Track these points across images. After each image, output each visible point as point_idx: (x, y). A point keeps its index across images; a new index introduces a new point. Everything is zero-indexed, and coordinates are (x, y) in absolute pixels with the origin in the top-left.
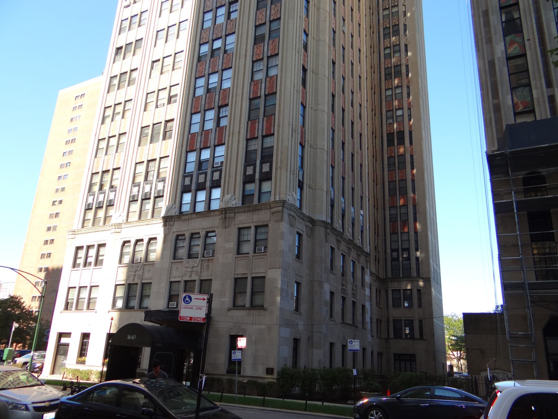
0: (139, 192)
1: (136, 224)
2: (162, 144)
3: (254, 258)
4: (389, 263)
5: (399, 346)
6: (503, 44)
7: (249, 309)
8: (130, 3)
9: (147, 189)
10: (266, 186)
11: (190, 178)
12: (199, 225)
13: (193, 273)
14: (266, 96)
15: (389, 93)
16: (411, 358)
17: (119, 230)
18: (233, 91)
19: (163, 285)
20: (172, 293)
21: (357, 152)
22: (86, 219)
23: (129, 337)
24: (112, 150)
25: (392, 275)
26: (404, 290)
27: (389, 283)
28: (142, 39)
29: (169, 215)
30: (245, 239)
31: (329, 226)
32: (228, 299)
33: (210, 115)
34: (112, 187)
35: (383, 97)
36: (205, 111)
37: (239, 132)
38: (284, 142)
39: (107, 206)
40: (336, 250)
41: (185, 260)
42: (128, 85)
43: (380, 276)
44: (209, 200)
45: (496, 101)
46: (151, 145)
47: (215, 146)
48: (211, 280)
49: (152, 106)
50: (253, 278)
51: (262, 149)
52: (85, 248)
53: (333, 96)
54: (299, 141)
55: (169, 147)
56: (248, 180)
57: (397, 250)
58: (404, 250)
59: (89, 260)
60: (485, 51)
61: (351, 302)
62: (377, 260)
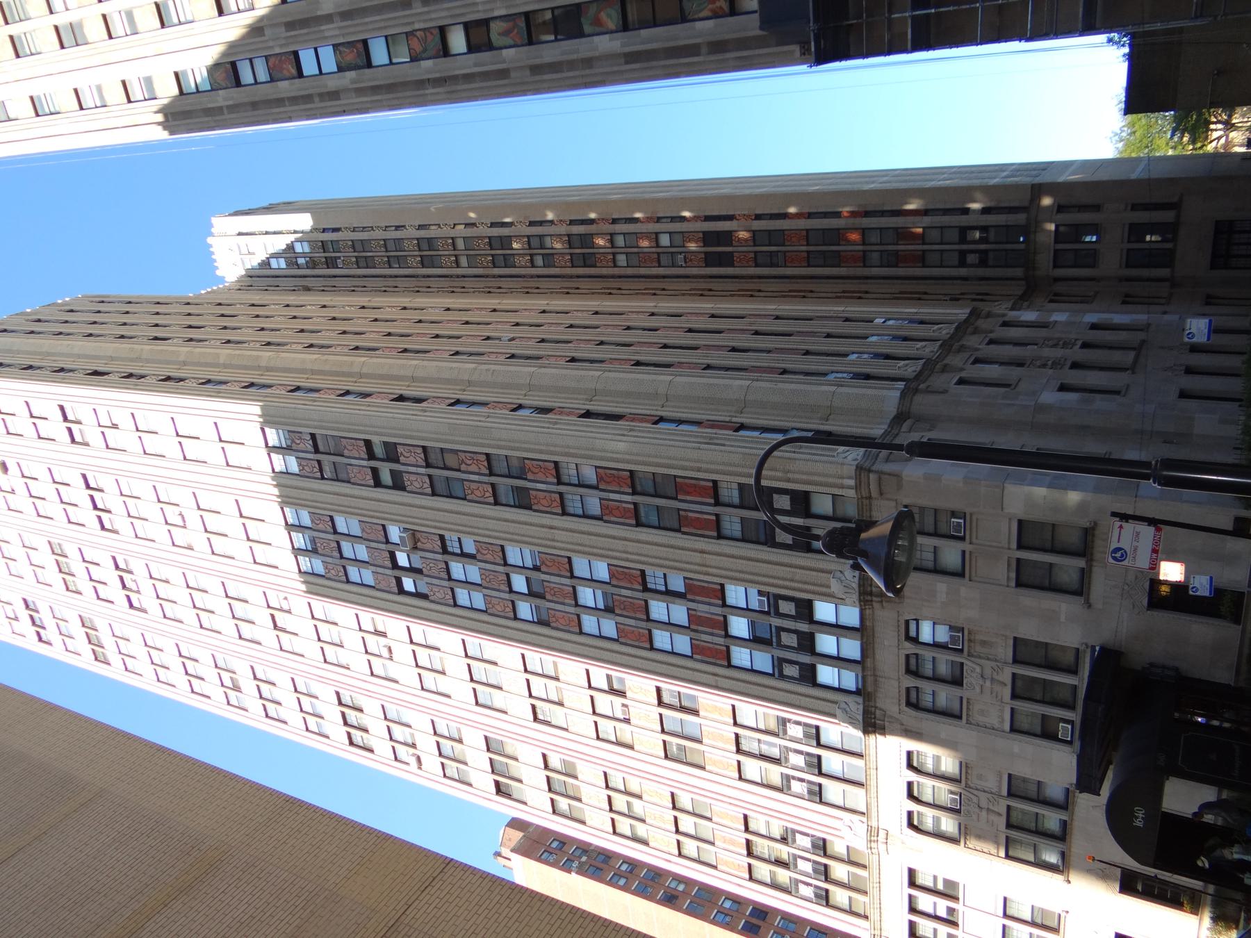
0: (802, 780)
1: (873, 795)
2: (705, 718)
3: (974, 540)
6: (596, 39)
7: (1090, 561)
8: (414, 755)
9: (799, 760)
10: (822, 505)
11: (784, 665)
12: (890, 655)
13: (995, 676)
14: (634, 493)
15: (622, 259)
17: (882, 834)
18: (616, 558)
19: (1016, 750)
20: (1038, 730)
21: (751, 324)
22: (847, 908)
23: (1139, 823)
24: (705, 828)
26: (1056, 242)
28: (486, 738)
29: (860, 718)
30: (930, 556)
31: (912, 387)
32: (1064, 606)
33: (658, 609)
34: (784, 840)
35: (630, 271)
36: (648, 619)
37: (702, 552)
38: (730, 462)
39: (825, 855)
40: (963, 374)
41: (965, 693)
42: (576, 777)
43: (1020, 293)
44: (837, 628)
45: (704, 50)
46: (704, 741)
47: (724, 605)
48: (1015, 639)
49: (625, 733)
50: (1020, 546)
51: (741, 506)
52: (914, 918)
53: (638, 363)
54: (731, 432)
55: (714, 706)
56: (803, 542)
57: (963, 254)
58: (963, 239)
59: (942, 913)
60: (608, 69)
61: (1085, 350)
62: (983, 297)
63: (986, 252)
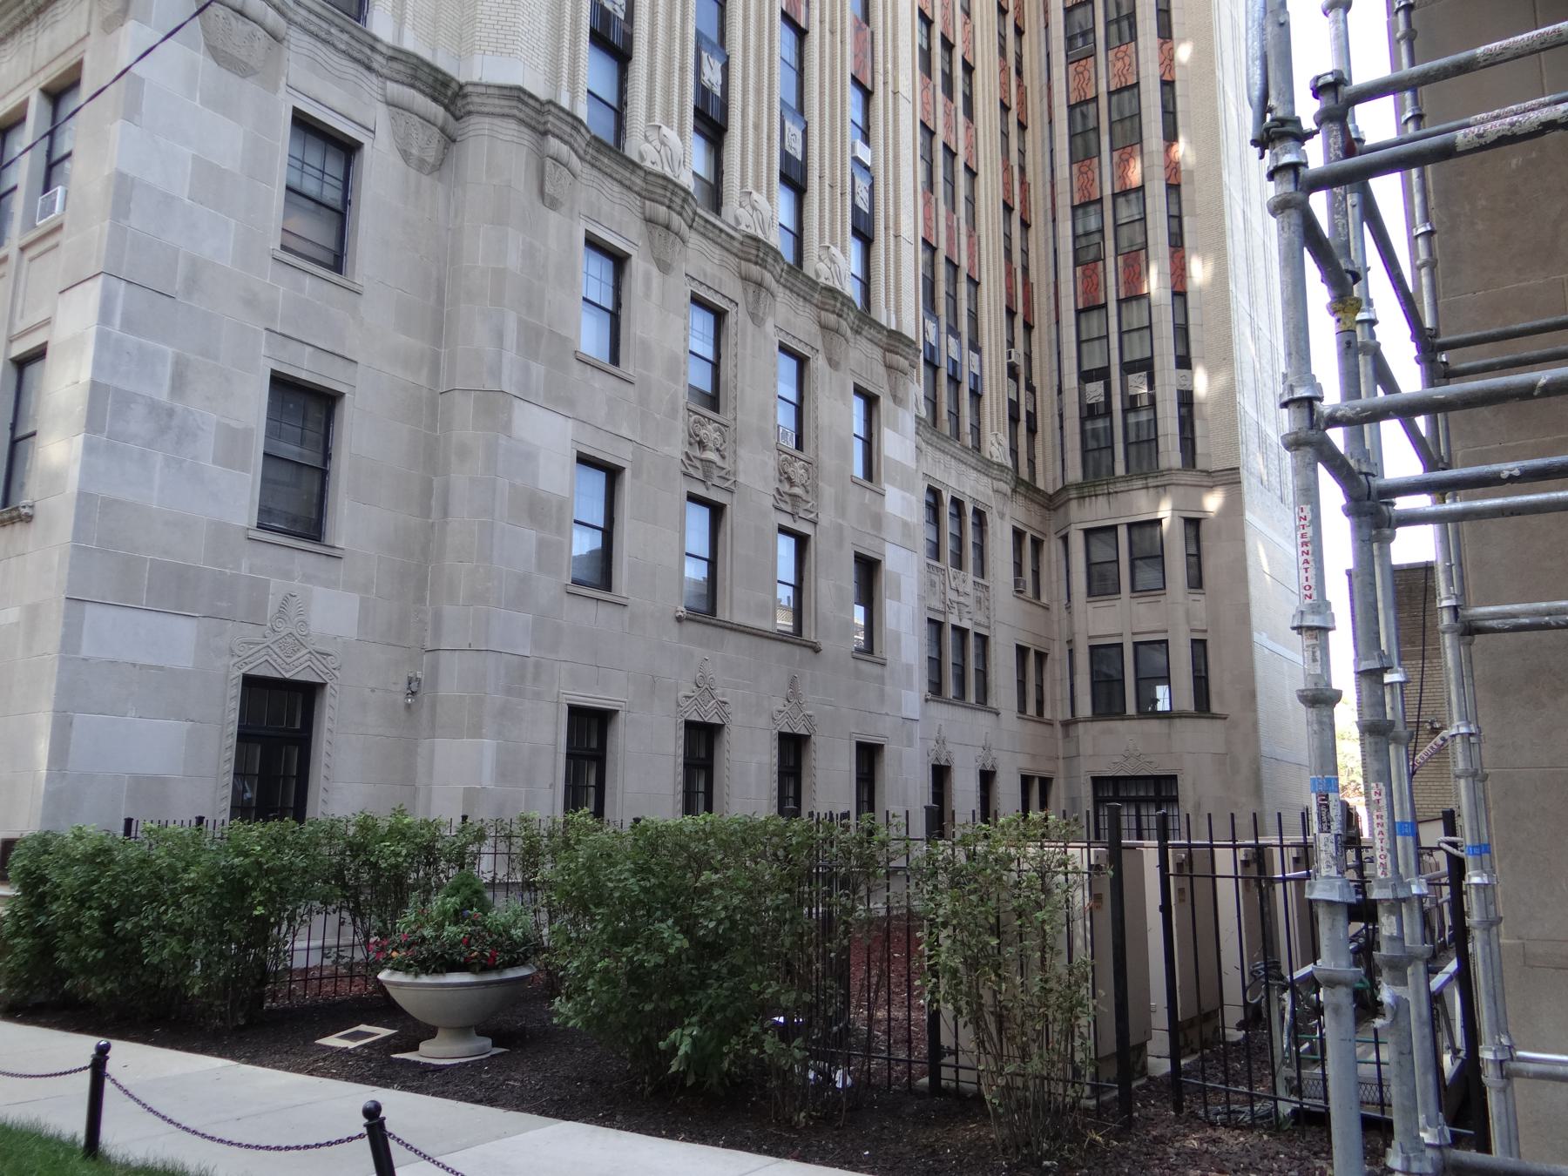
27: (1074, 504)
57: (1103, 374)
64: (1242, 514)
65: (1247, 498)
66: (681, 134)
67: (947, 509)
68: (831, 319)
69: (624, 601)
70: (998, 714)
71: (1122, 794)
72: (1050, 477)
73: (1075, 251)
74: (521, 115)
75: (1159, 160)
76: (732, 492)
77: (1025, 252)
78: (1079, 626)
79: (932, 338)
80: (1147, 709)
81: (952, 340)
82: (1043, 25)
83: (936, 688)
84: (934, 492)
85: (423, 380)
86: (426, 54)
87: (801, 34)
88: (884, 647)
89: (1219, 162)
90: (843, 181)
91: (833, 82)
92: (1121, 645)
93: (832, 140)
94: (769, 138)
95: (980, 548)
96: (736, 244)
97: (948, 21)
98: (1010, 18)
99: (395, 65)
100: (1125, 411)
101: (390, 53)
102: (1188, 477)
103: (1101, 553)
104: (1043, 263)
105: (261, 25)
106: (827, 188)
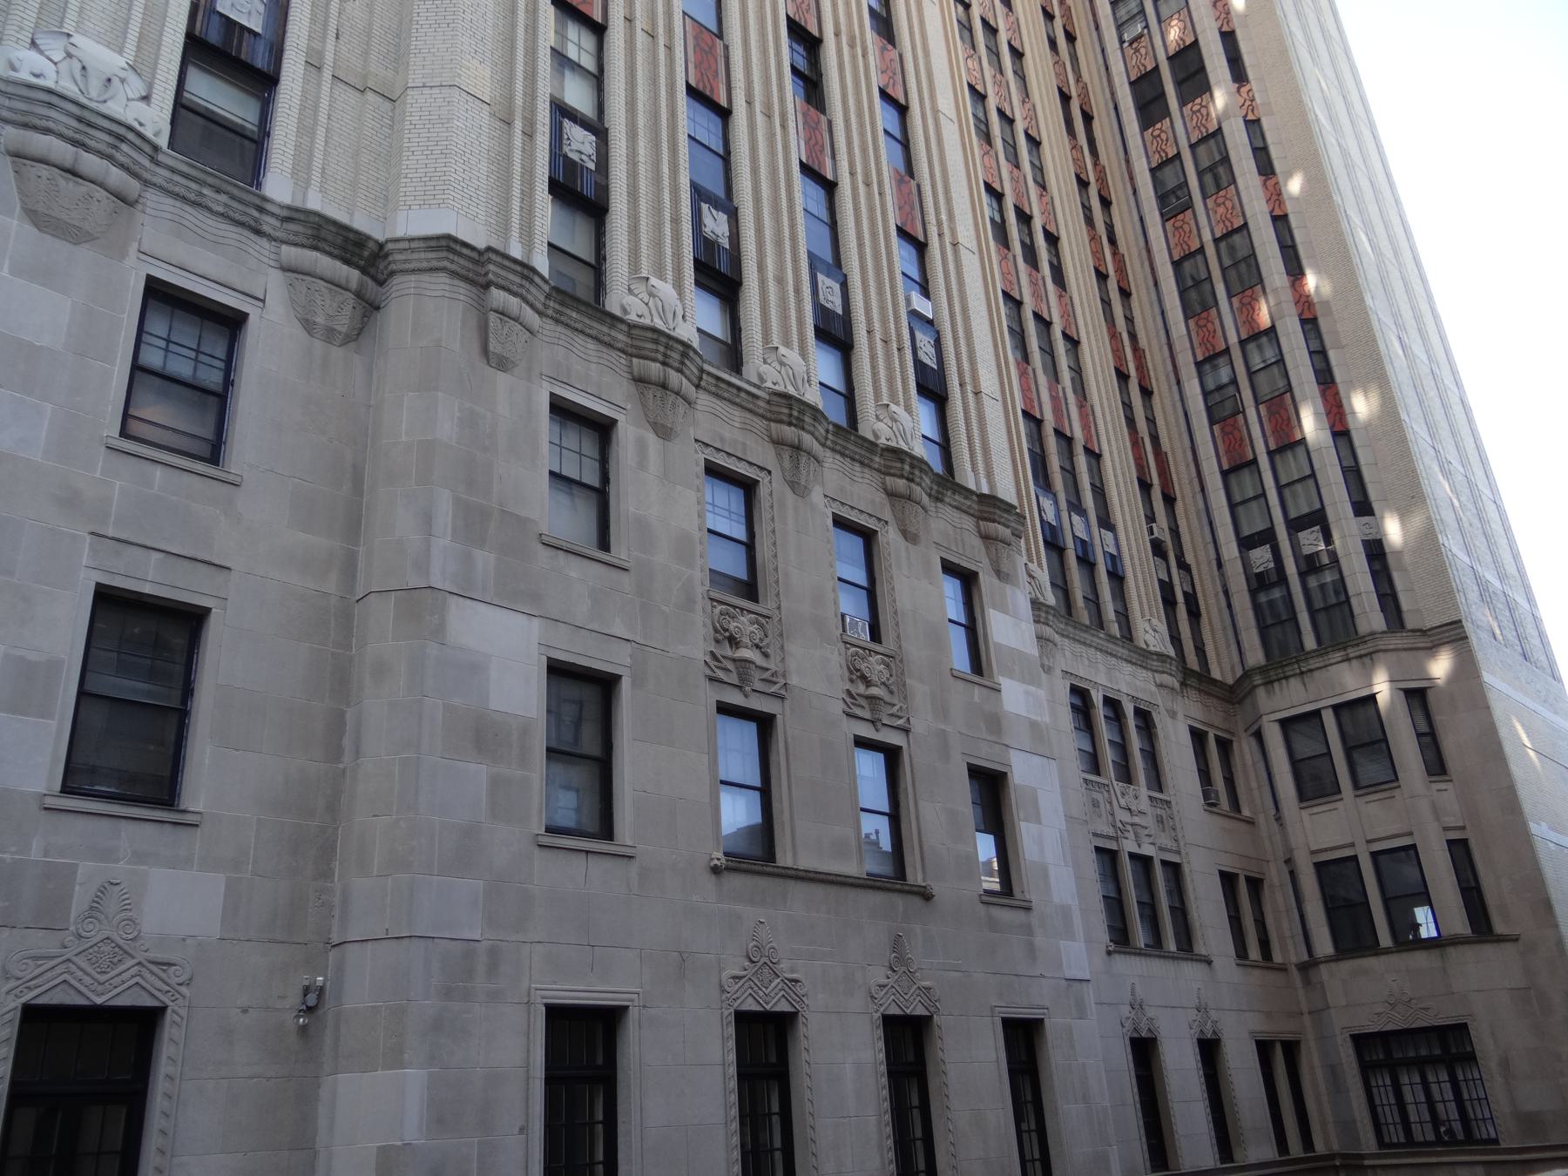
4: (1242, 601)
5: (1373, 993)
16: (1449, 1046)
25: (1268, 655)
27: (1261, 693)
63: (1282, 579)
64: (1479, 676)
65: (1480, 656)
66: (678, 285)
67: (1100, 711)
68: (901, 484)
69: (628, 852)
70: (1209, 963)
71: (1397, 1055)
72: (1227, 668)
73: (1209, 409)
74: (454, 267)
75: (1287, 296)
76: (782, 698)
77: (1151, 421)
78: (1297, 840)
79: (1050, 516)
80: (1406, 938)
81: (1076, 518)
82: (1130, 192)
83: (1121, 937)
84: (1080, 695)
85: (332, 585)
86: (341, 217)
87: (829, 187)
88: (1027, 886)
89: (1357, 286)
90: (899, 335)
91: (874, 235)
92: (1355, 858)
93: (881, 293)
94: (797, 291)
95: (1152, 756)
96: (761, 403)
97: (1021, 193)
98: (1093, 190)
99: (292, 226)
100: (1302, 575)
101: (285, 213)
102: (1396, 641)
103: (1307, 747)
104: (1174, 430)
105: (101, 185)
106: (879, 345)
